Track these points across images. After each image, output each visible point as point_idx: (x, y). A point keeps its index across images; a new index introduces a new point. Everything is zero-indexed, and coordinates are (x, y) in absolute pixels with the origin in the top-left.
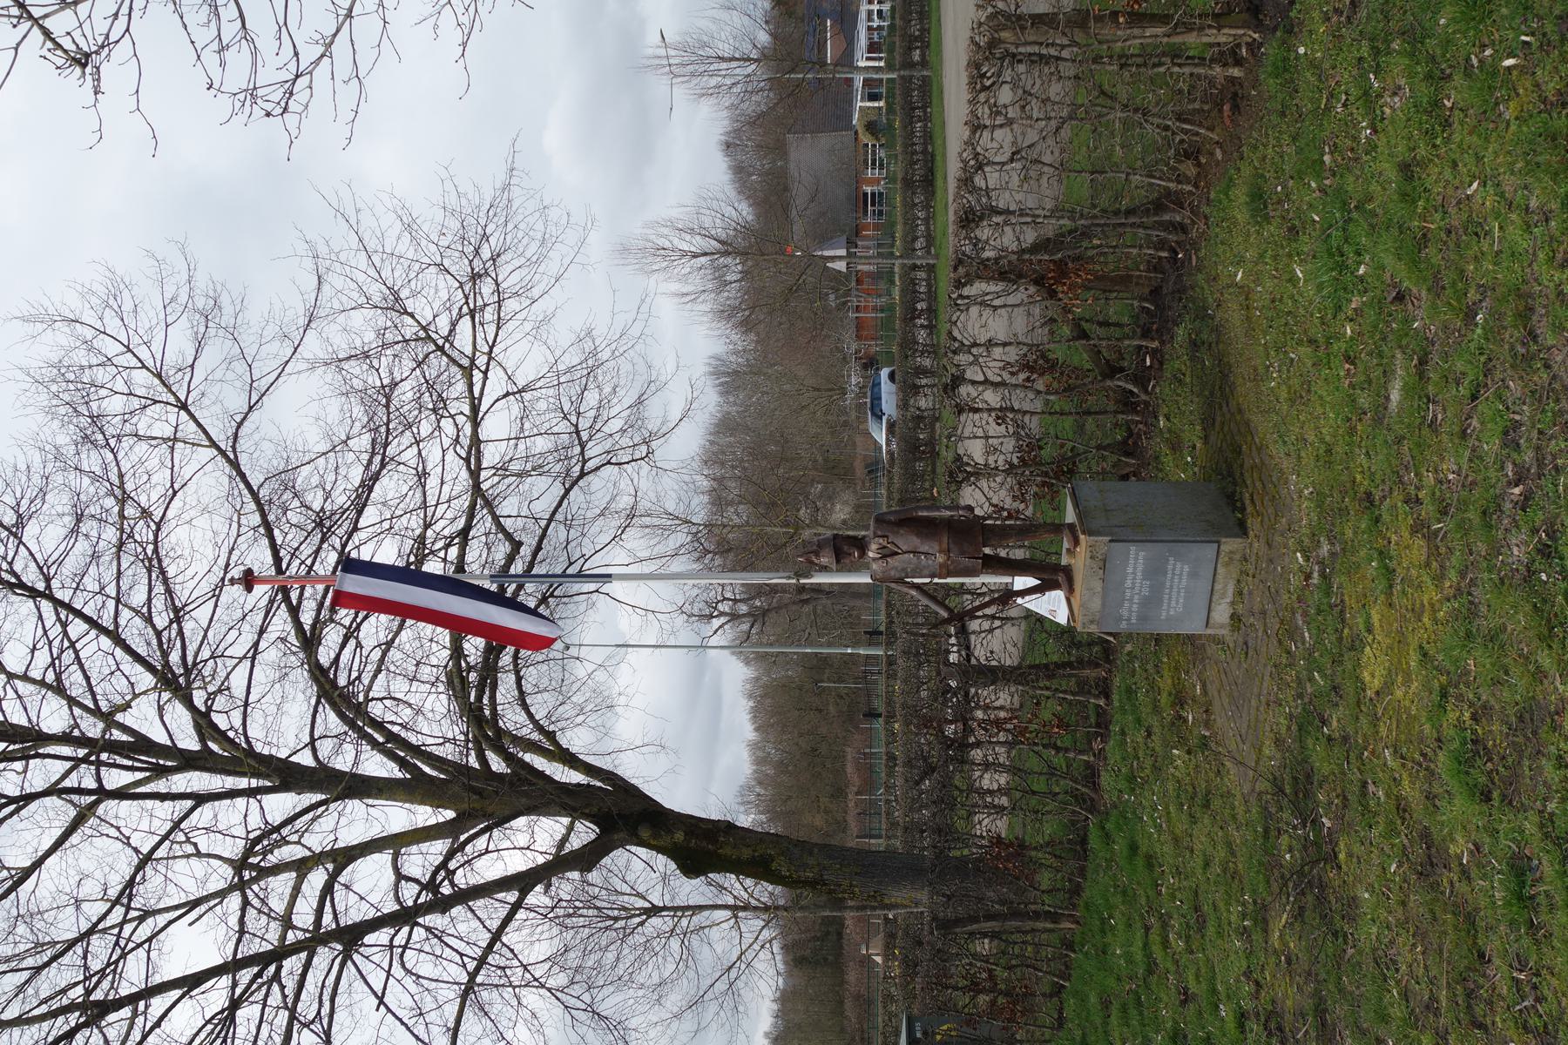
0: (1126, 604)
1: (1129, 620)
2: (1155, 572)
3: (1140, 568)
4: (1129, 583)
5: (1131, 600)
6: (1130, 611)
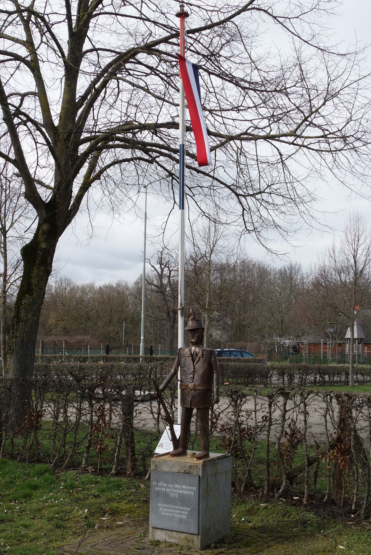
0: (165, 485)
1: (157, 486)
2: (183, 500)
3: (185, 492)
4: (177, 486)
5: (168, 487)
6: (162, 487)
